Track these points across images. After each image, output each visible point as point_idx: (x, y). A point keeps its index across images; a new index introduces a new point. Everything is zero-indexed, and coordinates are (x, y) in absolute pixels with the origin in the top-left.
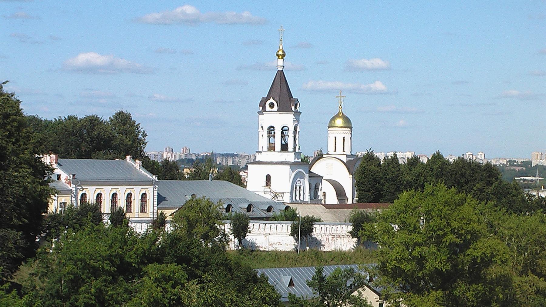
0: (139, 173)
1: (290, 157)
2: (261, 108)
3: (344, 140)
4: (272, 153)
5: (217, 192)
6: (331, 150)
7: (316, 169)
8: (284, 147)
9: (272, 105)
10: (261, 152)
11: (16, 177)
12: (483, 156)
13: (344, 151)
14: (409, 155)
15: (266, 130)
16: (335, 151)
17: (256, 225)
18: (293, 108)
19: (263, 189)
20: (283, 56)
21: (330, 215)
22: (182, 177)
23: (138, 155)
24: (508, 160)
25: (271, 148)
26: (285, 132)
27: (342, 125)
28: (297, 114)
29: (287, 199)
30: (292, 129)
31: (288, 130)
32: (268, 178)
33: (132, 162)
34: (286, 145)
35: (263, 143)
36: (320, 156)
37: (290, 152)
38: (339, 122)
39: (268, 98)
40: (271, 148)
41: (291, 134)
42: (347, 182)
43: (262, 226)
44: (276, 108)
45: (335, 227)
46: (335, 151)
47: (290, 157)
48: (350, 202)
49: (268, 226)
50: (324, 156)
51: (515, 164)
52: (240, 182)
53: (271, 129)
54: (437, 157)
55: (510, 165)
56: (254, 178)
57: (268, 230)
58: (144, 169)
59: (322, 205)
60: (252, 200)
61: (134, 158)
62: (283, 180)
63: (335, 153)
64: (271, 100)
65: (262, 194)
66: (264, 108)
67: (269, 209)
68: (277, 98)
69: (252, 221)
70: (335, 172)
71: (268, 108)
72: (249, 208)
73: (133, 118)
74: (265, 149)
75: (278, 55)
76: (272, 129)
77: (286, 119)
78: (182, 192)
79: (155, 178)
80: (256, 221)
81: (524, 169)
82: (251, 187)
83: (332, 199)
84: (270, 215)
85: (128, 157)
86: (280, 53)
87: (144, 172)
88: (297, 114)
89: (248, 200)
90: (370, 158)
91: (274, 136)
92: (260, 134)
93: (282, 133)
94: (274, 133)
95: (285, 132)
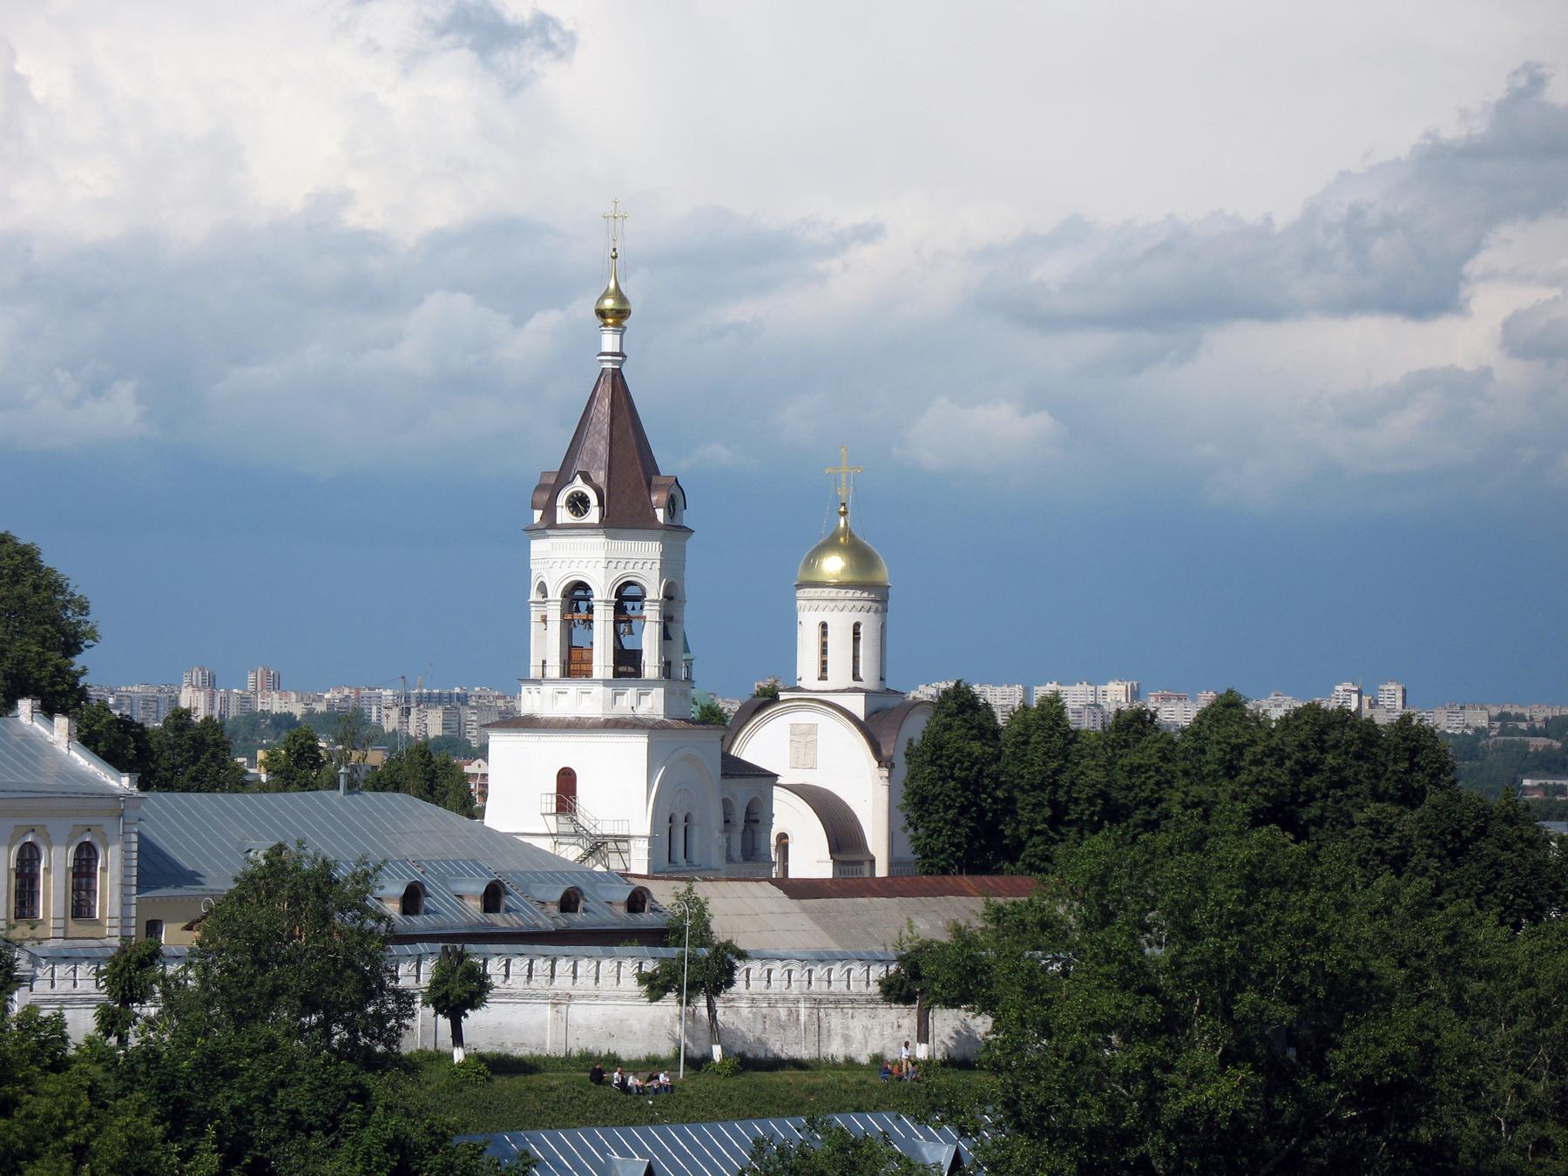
0: (81, 776)
1: (652, 704)
2: (538, 514)
3: (856, 634)
4: (573, 688)
5: (336, 828)
6: (807, 670)
7: (762, 745)
8: (627, 663)
9: (578, 504)
10: (537, 682)
11: (1122, 1095)
12: (1399, 695)
13: (856, 677)
14: (1115, 695)
15: (555, 593)
16: (823, 677)
17: (519, 965)
18: (660, 514)
19: (552, 824)
20: (621, 314)
21: (805, 922)
22: (240, 783)
23: (60, 696)
24: (1495, 711)
25: (575, 665)
26: (629, 605)
27: (848, 578)
28: (675, 531)
29: (638, 861)
30: (654, 591)
31: (640, 598)
32: (567, 781)
33: (39, 727)
34: (637, 654)
35: (546, 644)
36: (766, 700)
37: (652, 683)
38: (833, 565)
39: (563, 478)
40: (575, 665)
41: (651, 613)
42: (868, 794)
43: (541, 965)
44: (593, 515)
45: (819, 971)
46: (823, 677)
47: (652, 704)
48: (881, 871)
49: (563, 966)
50: (783, 696)
51: (1523, 726)
52: (468, 803)
53: (577, 594)
54: (1228, 707)
55: (1500, 734)
56: (514, 786)
57: (563, 983)
58: (86, 752)
59: (773, 882)
60: (501, 866)
61: (48, 710)
62: (621, 792)
63: (823, 685)
64: (579, 485)
65: (545, 844)
66: (550, 510)
67: (569, 902)
68: (600, 477)
69: (395, 950)
70: (823, 759)
71: (564, 516)
72: (493, 897)
73: (47, 560)
74: (554, 671)
75: (602, 314)
76: (579, 593)
77: (641, 559)
78: (223, 837)
79: (123, 783)
80: (539, 948)
81: (1557, 744)
82: (501, 815)
83: (810, 856)
84: (576, 921)
85: (25, 706)
86: (609, 304)
87: (84, 762)
88: (675, 531)
89: (486, 865)
90: (962, 706)
91: (589, 622)
92: (535, 616)
93: (619, 609)
94: (590, 610)
95: (629, 605)
